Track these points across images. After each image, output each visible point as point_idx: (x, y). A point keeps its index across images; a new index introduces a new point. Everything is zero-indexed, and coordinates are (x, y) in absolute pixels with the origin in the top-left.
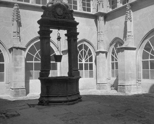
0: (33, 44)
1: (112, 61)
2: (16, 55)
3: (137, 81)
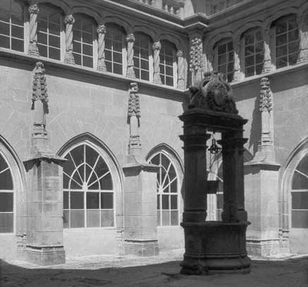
0: (68, 151)
1: (64, 188)
2: (47, 174)
3: (281, 232)
